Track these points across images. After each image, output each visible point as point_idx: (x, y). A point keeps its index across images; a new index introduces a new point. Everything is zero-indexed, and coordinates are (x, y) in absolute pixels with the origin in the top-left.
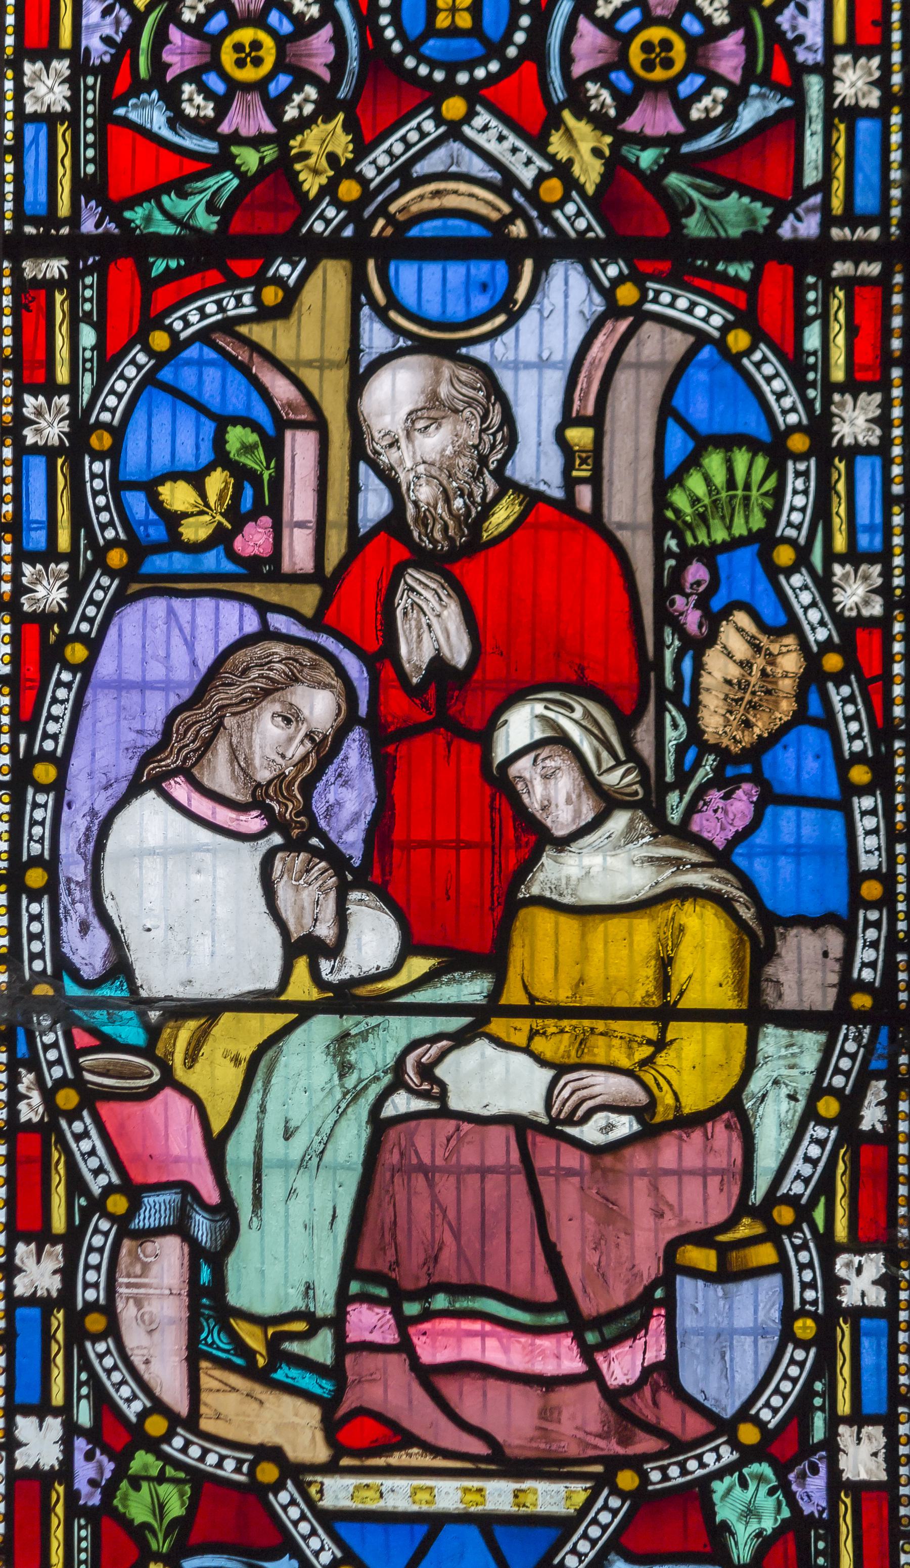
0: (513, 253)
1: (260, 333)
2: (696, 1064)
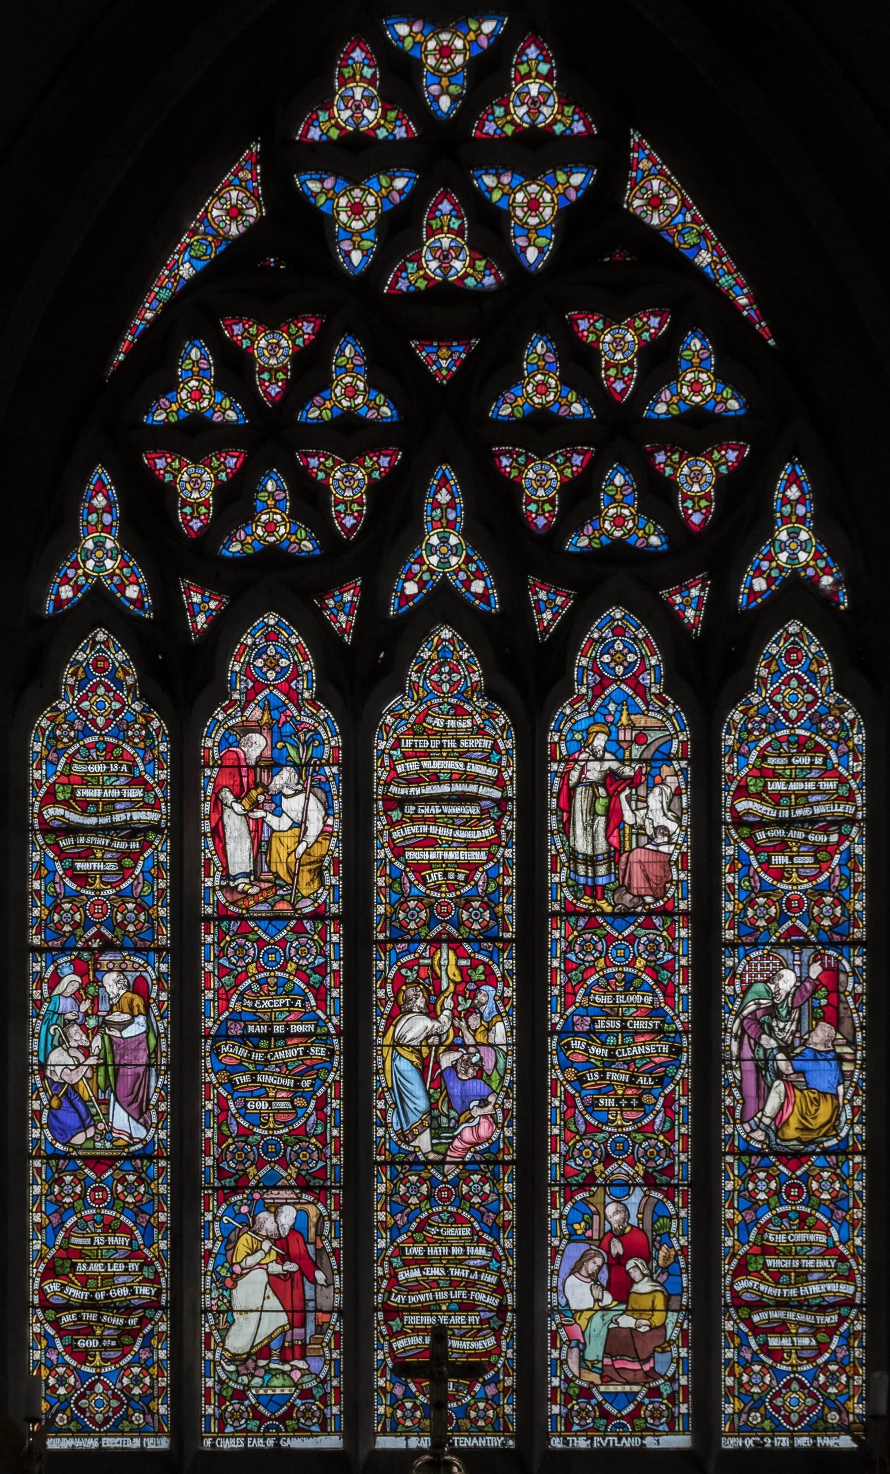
0: (629, 1186)
1: (590, 1199)
2: (658, 1319)
